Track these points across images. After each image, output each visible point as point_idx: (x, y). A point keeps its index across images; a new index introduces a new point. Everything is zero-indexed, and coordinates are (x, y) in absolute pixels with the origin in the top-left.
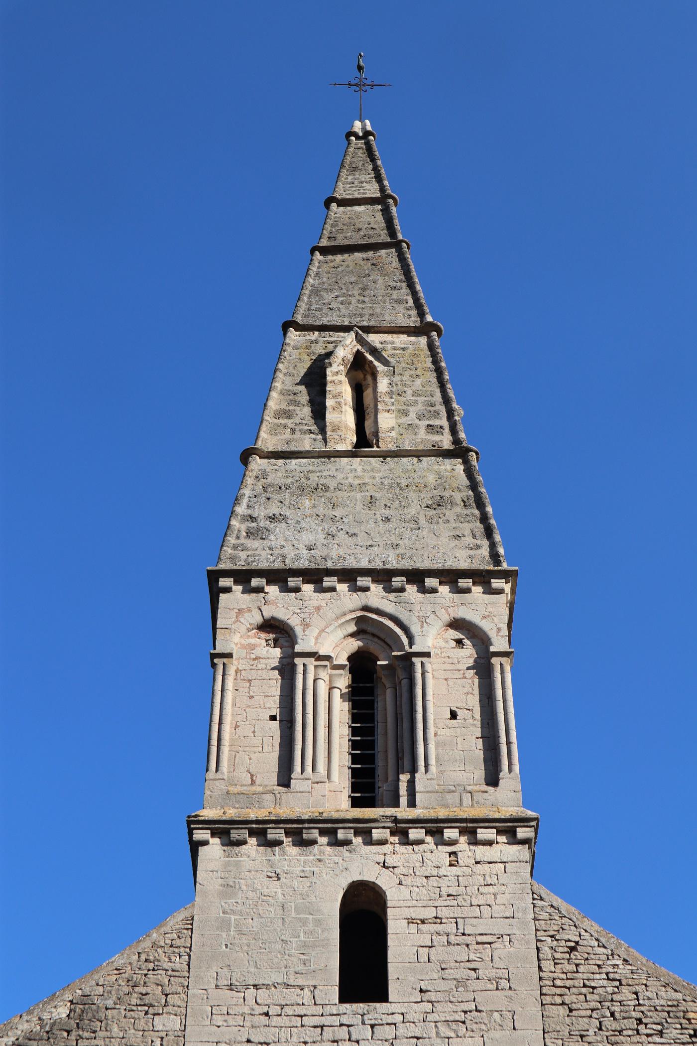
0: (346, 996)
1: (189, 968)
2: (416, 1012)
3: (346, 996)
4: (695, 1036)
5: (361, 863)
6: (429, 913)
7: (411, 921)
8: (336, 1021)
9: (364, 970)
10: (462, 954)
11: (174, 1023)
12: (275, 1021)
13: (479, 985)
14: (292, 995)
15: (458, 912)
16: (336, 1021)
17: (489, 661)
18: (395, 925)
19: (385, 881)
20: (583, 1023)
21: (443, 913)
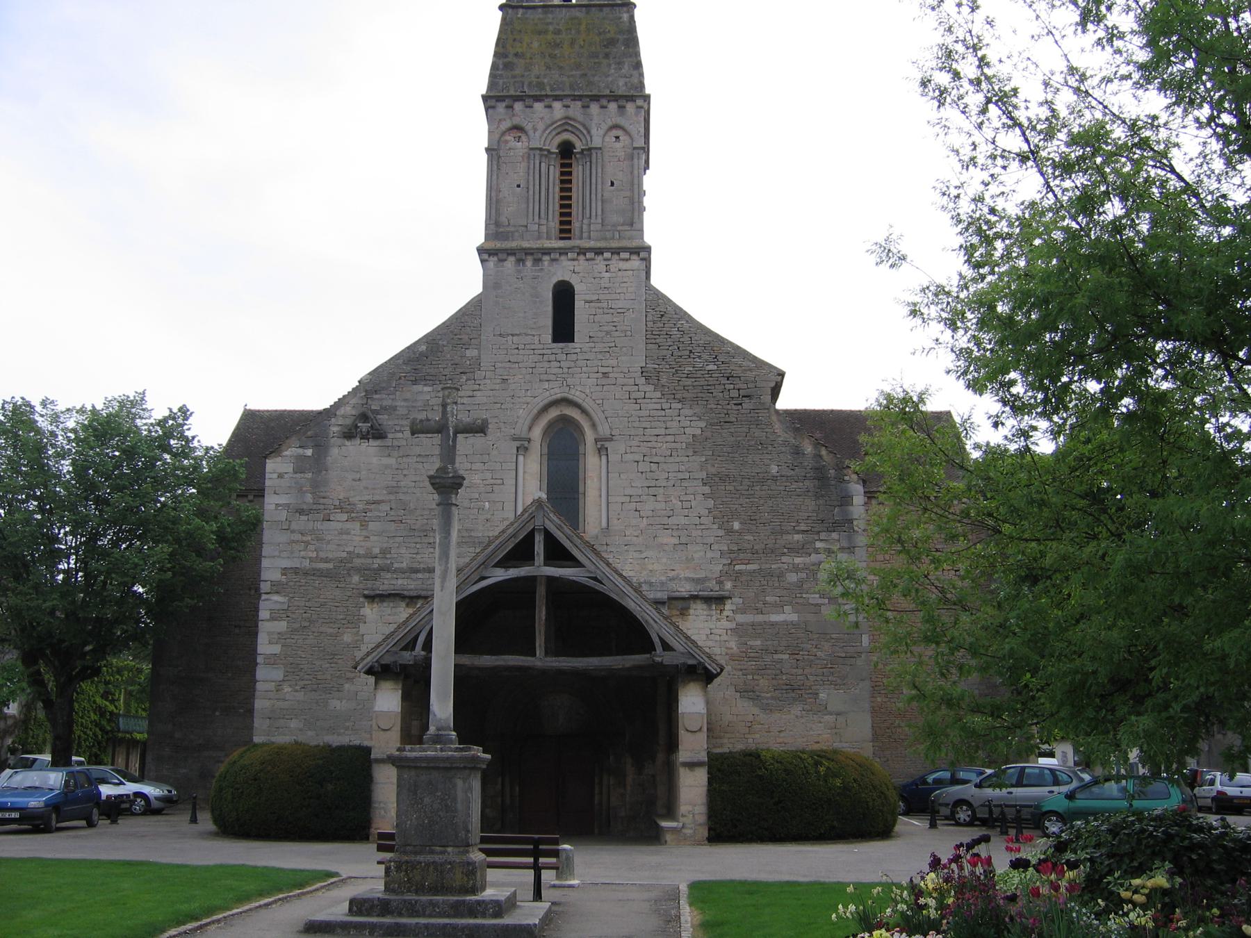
0: (555, 340)
1: (418, 597)
2: (586, 347)
3: (555, 340)
4: (1040, 935)
5: (563, 270)
6: (595, 297)
7: (586, 302)
8: (549, 352)
9: (563, 330)
10: (608, 318)
11: (475, 353)
12: (521, 352)
13: (617, 334)
14: (528, 339)
15: (608, 297)
16: (549, 352)
17: (777, 412)
18: (579, 304)
19: (574, 281)
20: (665, 352)
21: (601, 297)
